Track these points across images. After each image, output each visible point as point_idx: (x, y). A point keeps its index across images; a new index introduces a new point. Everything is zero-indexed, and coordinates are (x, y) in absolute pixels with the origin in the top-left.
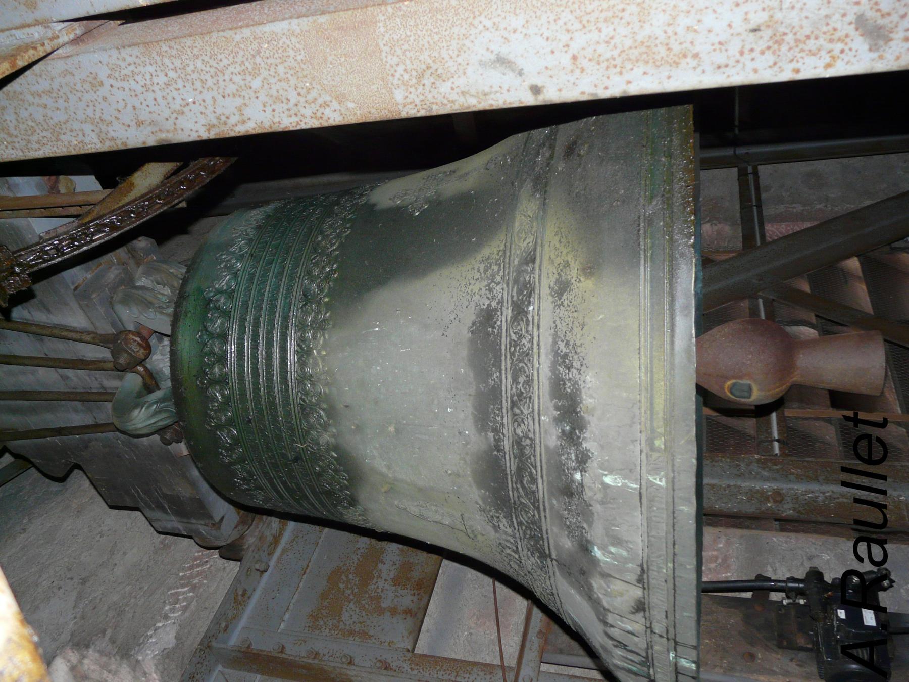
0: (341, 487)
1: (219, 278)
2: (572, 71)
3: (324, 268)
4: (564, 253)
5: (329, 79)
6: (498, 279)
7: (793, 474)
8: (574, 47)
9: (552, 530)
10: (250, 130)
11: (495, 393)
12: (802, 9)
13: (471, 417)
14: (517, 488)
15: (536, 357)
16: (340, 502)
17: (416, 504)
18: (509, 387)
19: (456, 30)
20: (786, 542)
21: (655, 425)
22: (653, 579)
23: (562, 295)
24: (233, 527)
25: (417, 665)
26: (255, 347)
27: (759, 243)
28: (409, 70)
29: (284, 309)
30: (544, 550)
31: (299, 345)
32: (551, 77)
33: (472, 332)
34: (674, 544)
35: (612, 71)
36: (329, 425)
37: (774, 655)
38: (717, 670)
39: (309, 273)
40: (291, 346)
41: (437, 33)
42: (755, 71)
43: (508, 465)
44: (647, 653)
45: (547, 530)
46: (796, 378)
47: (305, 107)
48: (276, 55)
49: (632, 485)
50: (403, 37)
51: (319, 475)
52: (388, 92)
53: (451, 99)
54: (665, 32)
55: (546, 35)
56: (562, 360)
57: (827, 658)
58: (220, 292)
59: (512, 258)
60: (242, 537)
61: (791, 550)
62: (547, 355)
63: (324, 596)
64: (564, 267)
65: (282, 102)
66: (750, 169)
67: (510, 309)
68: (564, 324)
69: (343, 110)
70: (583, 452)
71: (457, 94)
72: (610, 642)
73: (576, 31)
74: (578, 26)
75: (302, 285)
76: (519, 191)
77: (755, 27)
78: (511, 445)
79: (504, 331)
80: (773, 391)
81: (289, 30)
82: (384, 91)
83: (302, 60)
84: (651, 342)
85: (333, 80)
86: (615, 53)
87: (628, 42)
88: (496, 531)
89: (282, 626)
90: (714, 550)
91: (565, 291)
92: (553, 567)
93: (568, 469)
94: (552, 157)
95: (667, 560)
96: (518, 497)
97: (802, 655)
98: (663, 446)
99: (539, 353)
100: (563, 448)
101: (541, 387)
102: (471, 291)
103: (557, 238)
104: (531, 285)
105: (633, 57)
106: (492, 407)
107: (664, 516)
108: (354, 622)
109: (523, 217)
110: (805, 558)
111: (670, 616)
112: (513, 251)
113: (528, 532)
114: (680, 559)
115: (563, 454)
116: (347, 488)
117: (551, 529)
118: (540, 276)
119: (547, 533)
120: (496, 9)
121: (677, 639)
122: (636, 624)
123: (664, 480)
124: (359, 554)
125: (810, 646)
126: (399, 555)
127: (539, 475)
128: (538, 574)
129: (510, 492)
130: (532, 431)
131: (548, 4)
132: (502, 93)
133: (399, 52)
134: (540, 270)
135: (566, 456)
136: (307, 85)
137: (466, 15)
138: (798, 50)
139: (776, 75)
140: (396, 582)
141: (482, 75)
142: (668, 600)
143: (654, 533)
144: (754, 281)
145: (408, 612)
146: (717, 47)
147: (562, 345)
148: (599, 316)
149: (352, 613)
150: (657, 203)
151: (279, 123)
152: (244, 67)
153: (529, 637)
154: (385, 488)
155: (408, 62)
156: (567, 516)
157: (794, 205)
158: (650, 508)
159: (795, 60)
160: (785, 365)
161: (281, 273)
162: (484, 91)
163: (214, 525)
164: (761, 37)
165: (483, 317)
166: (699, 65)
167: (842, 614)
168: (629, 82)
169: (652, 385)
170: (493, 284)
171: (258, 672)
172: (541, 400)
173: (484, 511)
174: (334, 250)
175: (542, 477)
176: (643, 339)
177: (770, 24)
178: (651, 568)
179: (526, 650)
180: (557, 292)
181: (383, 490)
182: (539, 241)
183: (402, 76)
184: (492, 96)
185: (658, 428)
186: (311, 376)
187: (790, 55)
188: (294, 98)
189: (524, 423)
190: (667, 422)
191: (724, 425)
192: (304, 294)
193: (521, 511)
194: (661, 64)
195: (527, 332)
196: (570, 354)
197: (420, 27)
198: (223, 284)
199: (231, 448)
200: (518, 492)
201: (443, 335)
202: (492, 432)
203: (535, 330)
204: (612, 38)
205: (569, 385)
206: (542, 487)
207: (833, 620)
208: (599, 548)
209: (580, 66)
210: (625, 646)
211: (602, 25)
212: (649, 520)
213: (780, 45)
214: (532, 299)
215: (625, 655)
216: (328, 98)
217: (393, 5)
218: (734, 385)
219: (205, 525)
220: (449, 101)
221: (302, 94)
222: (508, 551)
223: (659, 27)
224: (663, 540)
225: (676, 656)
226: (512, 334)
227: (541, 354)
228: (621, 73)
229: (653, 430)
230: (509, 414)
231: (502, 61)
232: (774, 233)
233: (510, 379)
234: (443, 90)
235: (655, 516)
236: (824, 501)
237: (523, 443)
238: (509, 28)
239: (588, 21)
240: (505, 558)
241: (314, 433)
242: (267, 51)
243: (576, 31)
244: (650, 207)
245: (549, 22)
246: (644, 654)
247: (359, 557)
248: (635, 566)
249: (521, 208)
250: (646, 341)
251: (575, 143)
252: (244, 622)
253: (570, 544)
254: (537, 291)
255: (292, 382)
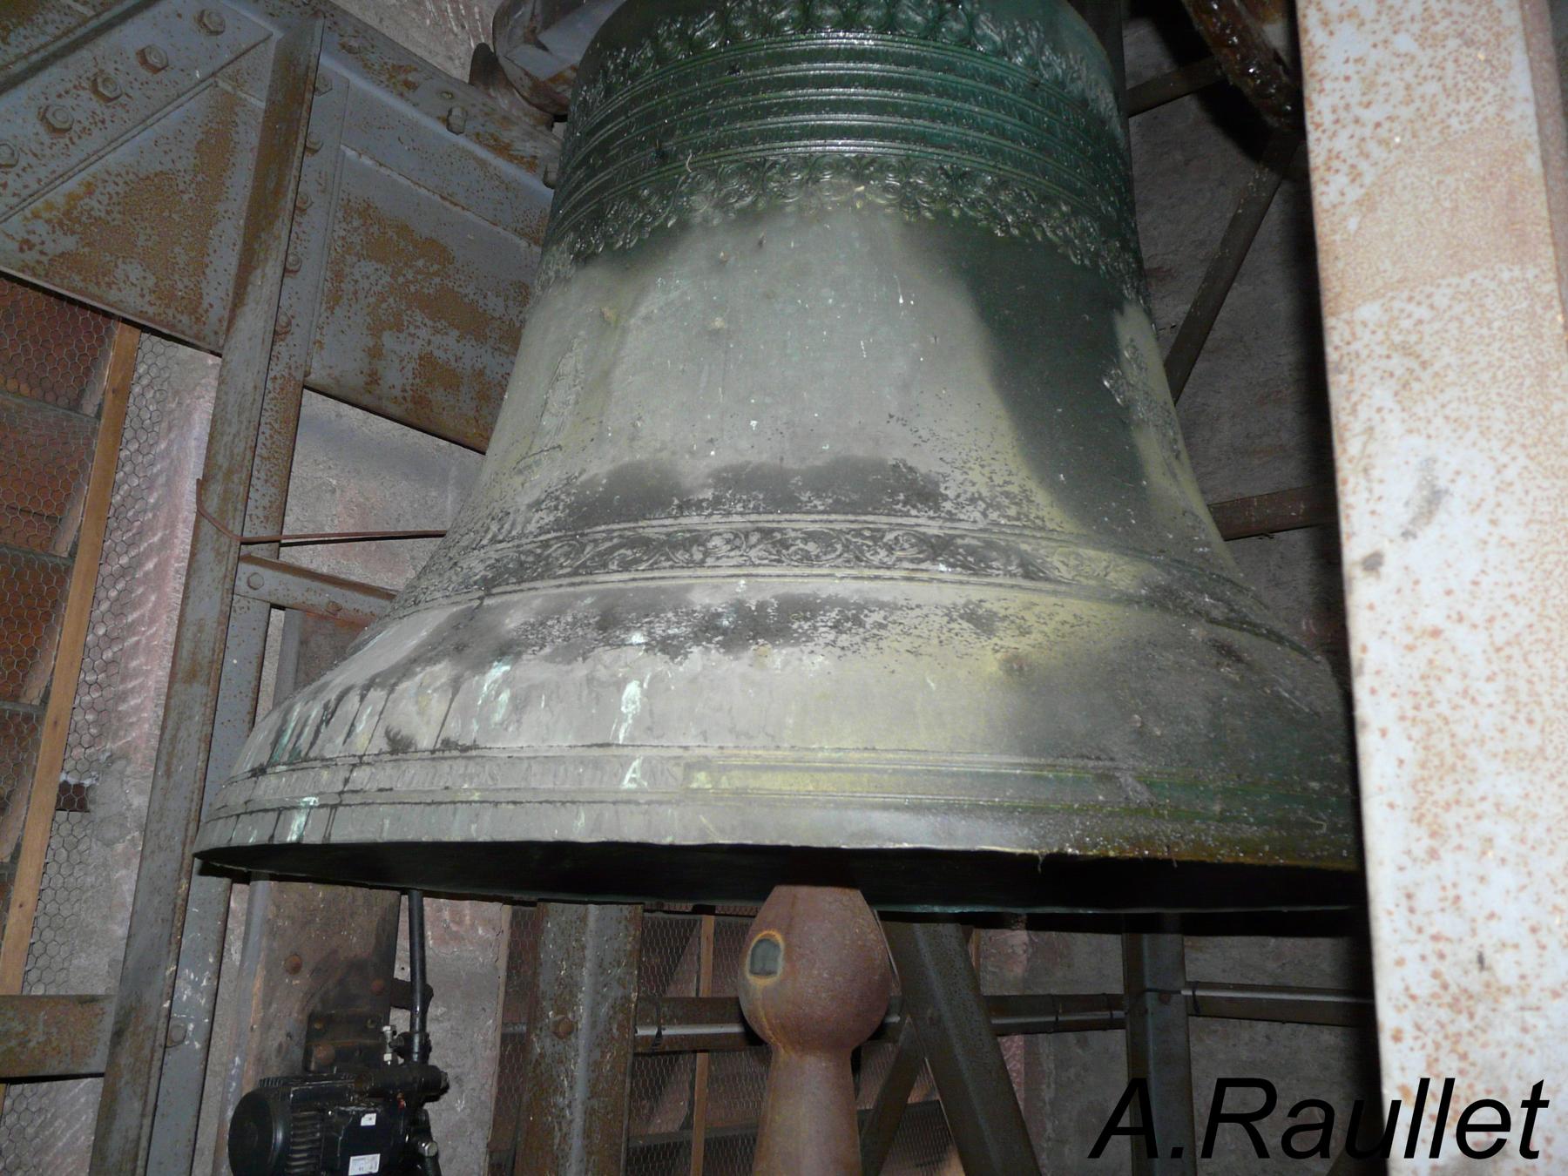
0: (611, 236)
1: (996, 21)
2: (1409, 629)
3: (1013, 212)
4: (1044, 628)
5: (1408, 181)
6: (994, 515)
7: (603, 1054)
8: (1458, 634)
9: (536, 597)
10: (1310, 36)
11: (787, 502)
12: (1521, 1046)
13: (741, 460)
14: (611, 539)
15: (854, 572)
16: (582, 236)
17: (580, 367)
18: (797, 526)
19: (1500, 413)
20: (485, 1041)
21: (735, 773)
22: (451, 767)
23: (969, 621)
24: (527, 69)
25: (282, 389)
26: (870, 82)
27: (995, 1021)
28: (1420, 328)
29: (939, 135)
30: (499, 585)
31: (873, 161)
32: (1399, 591)
33: (896, 467)
34: (514, 803)
35: (1408, 703)
36: (726, 213)
37: (297, 1007)
38: (273, 908)
39: (1003, 184)
40: (871, 147)
41: (1494, 377)
42: (1400, 962)
43: (654, 523)
44: (315, 759)
45: (536, 589)
46: (784, 1055)
47: (1352, 137)
48: (1460, 78)
49: (622, 731)
50: (1489, 315)
51: (634, 197)
52: (1377, 291)
53: (1359, 407)
54: (1483, 799)
55: (1486, 582)
56: (851, 616)
57: (294, 1092)
58: (972, 23)
59: (1031, 540)
60: (509, 85)
61: (472, 1049)
62: (858, 591)
63: (404, 230)
64: (1020, 627)
65: (1364, 94)
66: (1118, 1014)
67: (940, 533)
68: (916, 622)
69: (1343, 209)
70: (683, 647)
71: (1369, 420)
72: (333, 697)
73: (1491, 636)
74: (1500, 638)
75: (982, 171)
76: (1150, 561)
77: (1487, 962)
78: (691, 527)
79: (900, 520)
80: (762, 1013)
81: (1512, 99)
82: (1379, 283)
83: (1449, 127)
84: (885, 771)
85: (1405, 188)
86: (1444, 708)
87: (1464, 732)
88: (530, 507)
89: (350, 153)
90: (473, 919)
91: (975, 625)
92: (469, 601)
93: (650, 623)
94: (1213, 621)
95: (487, 790)
96: (595, 541)
97: (298, 1054)
98: (695, 785)
99: (862, 578)
100: (687, 614)
101: (800, 580)
102: (970, 468)
103: (1070, 619)
104: (984, 569)
105: (1434, 740)
106: (761, 496)
107: (567, 786)
108: (356, 282)
109: (1104, 564)
110: (459, 1070)
111: (384, 796)
112: (1044, 543)
113: (531, 559)
114: (488, 813)
115: (676, 614)
116: (608, 246)
117: (541, 595)
118: (1000, 585)
119: (530, 589)
120: (1539, 487)
121: (341, 809)
122: (367, 737)
123: (633, 786)
124: (476, 297)
125: (313, 1067)
126: (473, 366)
127: (638, 575)
128: (454, 578)
129: (603, 527)
130: (718, 564)
131: (1548, 583)
132: (1368, 500)
133: (1458, 309)
134: (1012, 586)
135: (674, 619)
136: (1397, 140)
137: (1530, 431)
138: (1439, 1037)
139: (1390, 999)
140: (426, 360)
141: (1407, 463)
142: (414, 791)
143: (535, 768)
144: (929, 1011)
145: (374, 379)
146: (1451, 893)
147: (878, 616)
148: (933, 681)
149: (373, 279)
150: (1141, 795)
151: (1321, 91)
152: (1438, 16)
153: (330, 588)
154: (609, 313)
155: (1437, 326)
156: (563, 621)
157: (1053, 1086)
158: (582, 761)
159: (1418, 1033)
160: (806, 1037)
161: (1003, 134)
162: (1373, 467)
163: (533, 31)
164: (1466, 972)
165: (924, 487)
166: (1415, 860)
167: (369, 1120)
168: (1384, 733)
169: (808, 769)
170: (984, 506)
171: (271, 102)
172: (776, 580)
173: (568, 484)
174: (1044, 233)
175: (634, 580)
176: (891, 756)
177: (1493, 990)
178: (472, 764)
179: (307, 582)
180: (973, 612)
181: (605, 310)
182: (1063, 588)
183: (1409, 316)
184: (1363, 483)
185: (728, 779)
186: (817, 181)
187: (1429, 1024)
188: (1369, 116)
189: (732, 550)
190: (740, 793)
191: (684, 948)
192: (965, 173)
193: (570, 545)
194: (1418, 792)
195: (900, 560)
196: (861, 630)
197: (1509, 346)
198: (986, 28)
199: (684, 38)
200: (604, 540)
201: (891, 416)
202: (715, 497)
203: (904, 573)
204: (1473, 700)
205: (806, 627)
206: (614, 580)
207: (358, 1105)
208: (506, 674)
209: (1419, 643)
210: (326, 720)
211: (1501, 682)
212: (559, 760)
213: (1450, 1006)
214: (959, 569)
215: (310, 722)
216: (1368, 179)
217: (1556, 294)
218: (776, 946)
219: (533, 14)
220: (1355, 404)
221: (1379, 130)
222: (494, 527)
223: (1494, 786)
224: (523, 785)
225: (311, 807)
226: (895, 534)
227: (860, 582)
228: (1403, 718)
229: (724, 769)
230: (749, 525)
231: (1432, 500)
232: (1010, 1048)
233: (815, 527)
234: (1377, 392)
235: (566, 770)
236: (555, 1105)
237: (695, 548)
238: (1499, 512)
239: (1509, 658)
240: (480, 524)
241: (711, 186)
242: (1470, 60)
243: (1491, 636)
244: (1130, 780)
245: (1510, 585)
246: (312, 755)
247: (471, 296)
248: (474, 735)
249: (1121, 562)
250: (890, 762)
251: (1239, 660)
252: (359, 82)
253: (512, 626)
254: (973, 579)
255: (806, 146)
